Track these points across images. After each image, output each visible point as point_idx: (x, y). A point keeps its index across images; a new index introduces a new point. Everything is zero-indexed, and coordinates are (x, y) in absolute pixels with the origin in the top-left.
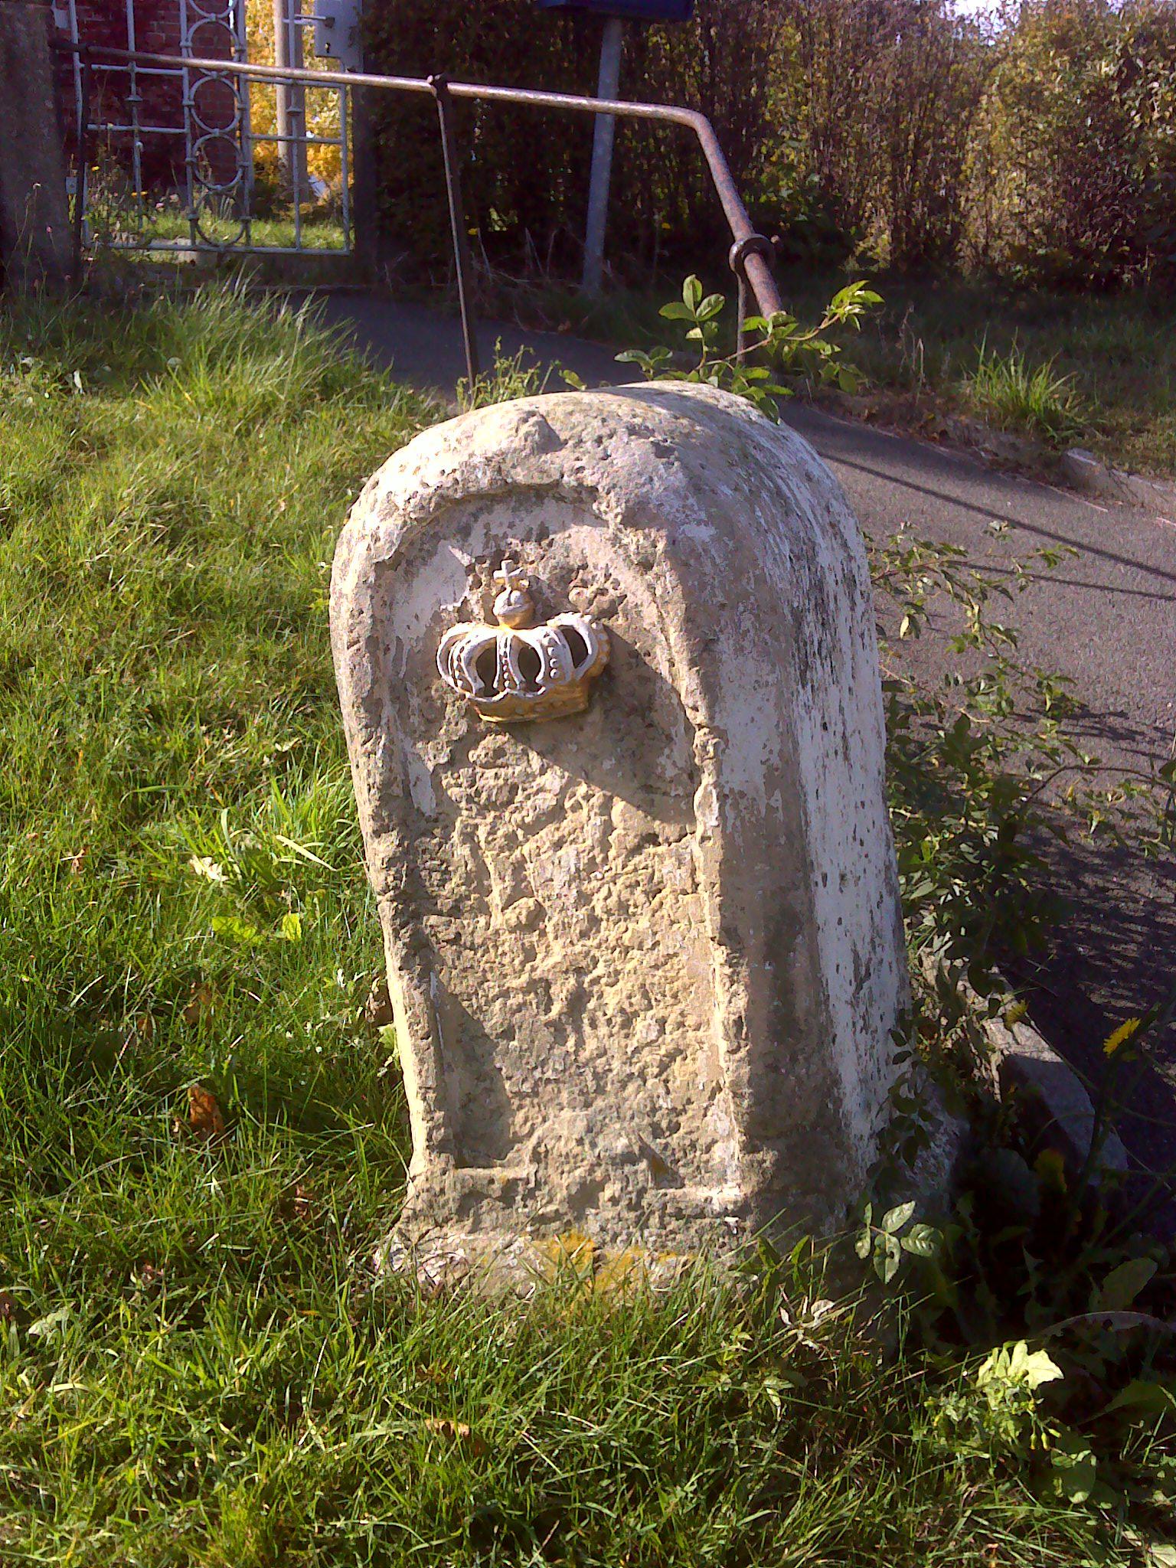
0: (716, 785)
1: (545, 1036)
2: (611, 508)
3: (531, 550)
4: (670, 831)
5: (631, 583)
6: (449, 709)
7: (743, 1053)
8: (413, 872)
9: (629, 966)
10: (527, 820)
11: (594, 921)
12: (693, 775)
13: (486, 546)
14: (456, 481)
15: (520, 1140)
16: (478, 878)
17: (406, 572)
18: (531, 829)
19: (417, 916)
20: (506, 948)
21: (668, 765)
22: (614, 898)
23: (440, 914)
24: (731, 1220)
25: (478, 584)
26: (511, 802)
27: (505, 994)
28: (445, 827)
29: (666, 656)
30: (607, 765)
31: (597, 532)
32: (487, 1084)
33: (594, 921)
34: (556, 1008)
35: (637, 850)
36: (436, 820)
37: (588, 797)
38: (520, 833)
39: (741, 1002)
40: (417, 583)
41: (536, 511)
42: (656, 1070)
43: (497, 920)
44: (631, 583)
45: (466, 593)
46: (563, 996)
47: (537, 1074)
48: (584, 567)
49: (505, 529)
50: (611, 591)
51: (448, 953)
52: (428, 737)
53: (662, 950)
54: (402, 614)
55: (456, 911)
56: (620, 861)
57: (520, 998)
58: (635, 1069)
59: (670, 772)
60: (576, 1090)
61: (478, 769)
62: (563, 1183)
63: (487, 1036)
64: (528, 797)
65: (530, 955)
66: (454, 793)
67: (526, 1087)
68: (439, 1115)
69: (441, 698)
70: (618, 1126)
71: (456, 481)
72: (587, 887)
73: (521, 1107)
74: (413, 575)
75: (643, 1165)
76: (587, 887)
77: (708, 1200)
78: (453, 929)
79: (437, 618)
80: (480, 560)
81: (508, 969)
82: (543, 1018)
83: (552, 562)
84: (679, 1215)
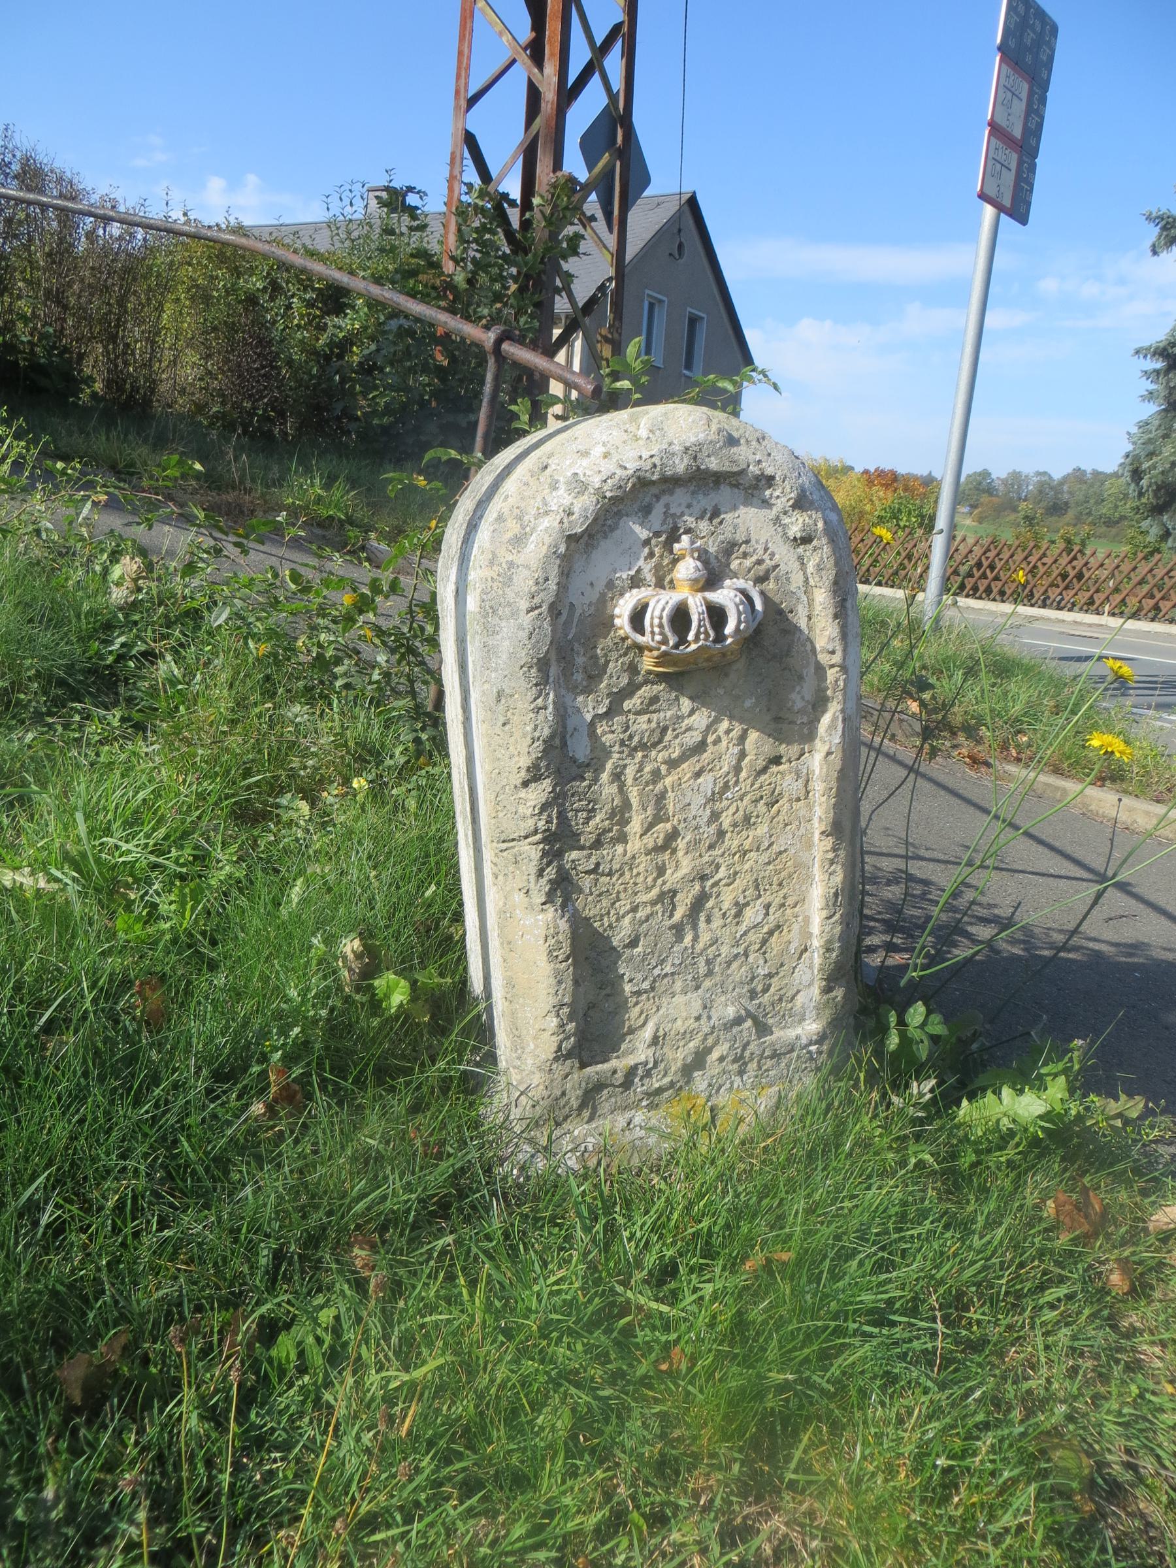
0: (843, 711)
1: (670, 936)
2: (782, 496)
3: (704, 526)
4: (794, 749)
5: (785, 556)
6: (611, 665)
7: (837, 916)
8: (561, 815)
9: (747, 866)
10: (673, 756)
11: (721, 834)
12: (819, 703)
13: (664, 522)
14: (655, 466)
15: (632, 1031)
16: (621, 814)
17: (587, 545)
18: (673, 764)
19: (559, 854)
20: (641, 868)
21: (798, 699)
22: (741, 813)
23: (582, 848)
24: (813, 1048)
25: (651, 555)
26: (660, 741)
27: (634, 909)
28: (596, 771)
29: (806, 613)
30: (748, 703)
31: (765, 512)
32: (608, 991)
33: (721, 834)
34: (678, 916)
35: (764, 770)
36: (588, 765)
37: (728, 732)
38: (664, 768)
39: (838, 878)
40: (596, 555)
41: (713, 495)
42: (757, 946)
43: (635, 845)
44: (785, 556)
45: (641, 562)
46: (688, 901)
47: (656, 972)
48: (747, 542)
49: (683, 508)
50: (768, 561)
51: (586, 882)
52: (587, 691)
53: (776, 848)
54: (578, 582)
55: (597, 844)
56: (749, 781)
57: (648, 910)
58: (741, 950)
59: (799, 704)
60: (690, 977)
61: (631, 716)
62: (678, 1056)
63: (614, 949)
64: (676, 737)
65: (661, 871)
66: (607, 739)
67: (646, 985)
68: (571, 1027)
69: (606, 655)
70: (723, 999)
71: (655, 466)
72: (718, 806)
73: (637, 1003)
74: (593, 547)
75: (749, 1023)
76: (718, 806)
77: (798, 1038)
78: (593, 860)
79: (610, 585)
80: (657, 534)
81: (640, 887)
82: (668, 923)
83: (721, 537)
84: (775, 1055)
